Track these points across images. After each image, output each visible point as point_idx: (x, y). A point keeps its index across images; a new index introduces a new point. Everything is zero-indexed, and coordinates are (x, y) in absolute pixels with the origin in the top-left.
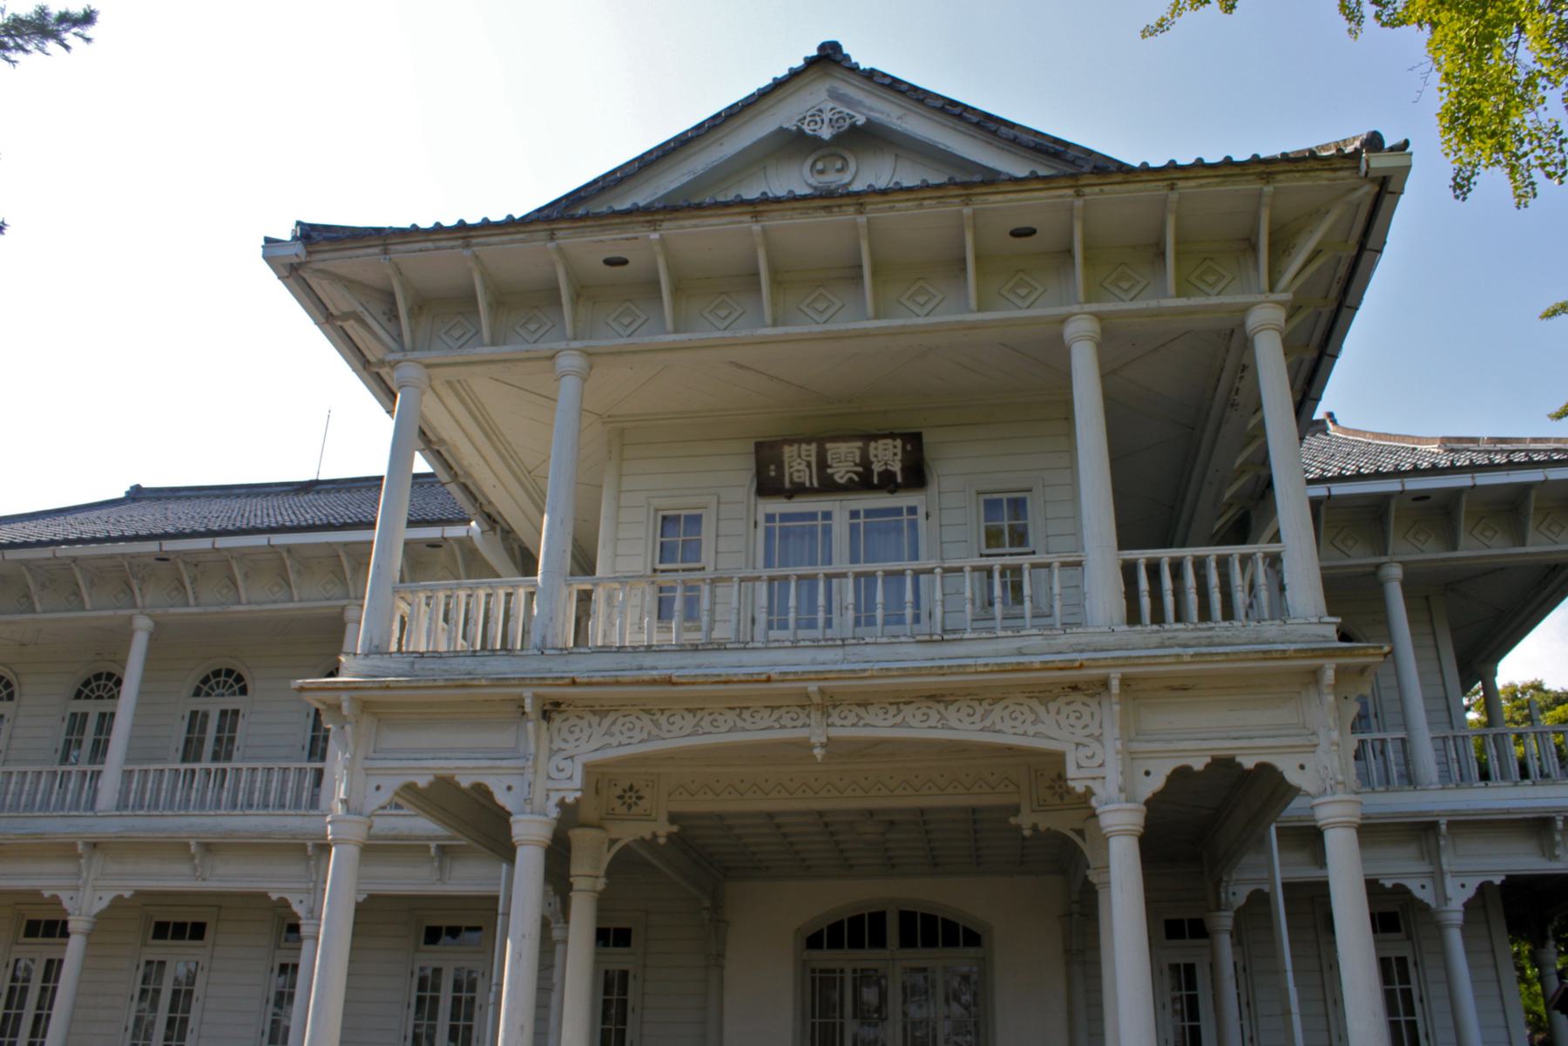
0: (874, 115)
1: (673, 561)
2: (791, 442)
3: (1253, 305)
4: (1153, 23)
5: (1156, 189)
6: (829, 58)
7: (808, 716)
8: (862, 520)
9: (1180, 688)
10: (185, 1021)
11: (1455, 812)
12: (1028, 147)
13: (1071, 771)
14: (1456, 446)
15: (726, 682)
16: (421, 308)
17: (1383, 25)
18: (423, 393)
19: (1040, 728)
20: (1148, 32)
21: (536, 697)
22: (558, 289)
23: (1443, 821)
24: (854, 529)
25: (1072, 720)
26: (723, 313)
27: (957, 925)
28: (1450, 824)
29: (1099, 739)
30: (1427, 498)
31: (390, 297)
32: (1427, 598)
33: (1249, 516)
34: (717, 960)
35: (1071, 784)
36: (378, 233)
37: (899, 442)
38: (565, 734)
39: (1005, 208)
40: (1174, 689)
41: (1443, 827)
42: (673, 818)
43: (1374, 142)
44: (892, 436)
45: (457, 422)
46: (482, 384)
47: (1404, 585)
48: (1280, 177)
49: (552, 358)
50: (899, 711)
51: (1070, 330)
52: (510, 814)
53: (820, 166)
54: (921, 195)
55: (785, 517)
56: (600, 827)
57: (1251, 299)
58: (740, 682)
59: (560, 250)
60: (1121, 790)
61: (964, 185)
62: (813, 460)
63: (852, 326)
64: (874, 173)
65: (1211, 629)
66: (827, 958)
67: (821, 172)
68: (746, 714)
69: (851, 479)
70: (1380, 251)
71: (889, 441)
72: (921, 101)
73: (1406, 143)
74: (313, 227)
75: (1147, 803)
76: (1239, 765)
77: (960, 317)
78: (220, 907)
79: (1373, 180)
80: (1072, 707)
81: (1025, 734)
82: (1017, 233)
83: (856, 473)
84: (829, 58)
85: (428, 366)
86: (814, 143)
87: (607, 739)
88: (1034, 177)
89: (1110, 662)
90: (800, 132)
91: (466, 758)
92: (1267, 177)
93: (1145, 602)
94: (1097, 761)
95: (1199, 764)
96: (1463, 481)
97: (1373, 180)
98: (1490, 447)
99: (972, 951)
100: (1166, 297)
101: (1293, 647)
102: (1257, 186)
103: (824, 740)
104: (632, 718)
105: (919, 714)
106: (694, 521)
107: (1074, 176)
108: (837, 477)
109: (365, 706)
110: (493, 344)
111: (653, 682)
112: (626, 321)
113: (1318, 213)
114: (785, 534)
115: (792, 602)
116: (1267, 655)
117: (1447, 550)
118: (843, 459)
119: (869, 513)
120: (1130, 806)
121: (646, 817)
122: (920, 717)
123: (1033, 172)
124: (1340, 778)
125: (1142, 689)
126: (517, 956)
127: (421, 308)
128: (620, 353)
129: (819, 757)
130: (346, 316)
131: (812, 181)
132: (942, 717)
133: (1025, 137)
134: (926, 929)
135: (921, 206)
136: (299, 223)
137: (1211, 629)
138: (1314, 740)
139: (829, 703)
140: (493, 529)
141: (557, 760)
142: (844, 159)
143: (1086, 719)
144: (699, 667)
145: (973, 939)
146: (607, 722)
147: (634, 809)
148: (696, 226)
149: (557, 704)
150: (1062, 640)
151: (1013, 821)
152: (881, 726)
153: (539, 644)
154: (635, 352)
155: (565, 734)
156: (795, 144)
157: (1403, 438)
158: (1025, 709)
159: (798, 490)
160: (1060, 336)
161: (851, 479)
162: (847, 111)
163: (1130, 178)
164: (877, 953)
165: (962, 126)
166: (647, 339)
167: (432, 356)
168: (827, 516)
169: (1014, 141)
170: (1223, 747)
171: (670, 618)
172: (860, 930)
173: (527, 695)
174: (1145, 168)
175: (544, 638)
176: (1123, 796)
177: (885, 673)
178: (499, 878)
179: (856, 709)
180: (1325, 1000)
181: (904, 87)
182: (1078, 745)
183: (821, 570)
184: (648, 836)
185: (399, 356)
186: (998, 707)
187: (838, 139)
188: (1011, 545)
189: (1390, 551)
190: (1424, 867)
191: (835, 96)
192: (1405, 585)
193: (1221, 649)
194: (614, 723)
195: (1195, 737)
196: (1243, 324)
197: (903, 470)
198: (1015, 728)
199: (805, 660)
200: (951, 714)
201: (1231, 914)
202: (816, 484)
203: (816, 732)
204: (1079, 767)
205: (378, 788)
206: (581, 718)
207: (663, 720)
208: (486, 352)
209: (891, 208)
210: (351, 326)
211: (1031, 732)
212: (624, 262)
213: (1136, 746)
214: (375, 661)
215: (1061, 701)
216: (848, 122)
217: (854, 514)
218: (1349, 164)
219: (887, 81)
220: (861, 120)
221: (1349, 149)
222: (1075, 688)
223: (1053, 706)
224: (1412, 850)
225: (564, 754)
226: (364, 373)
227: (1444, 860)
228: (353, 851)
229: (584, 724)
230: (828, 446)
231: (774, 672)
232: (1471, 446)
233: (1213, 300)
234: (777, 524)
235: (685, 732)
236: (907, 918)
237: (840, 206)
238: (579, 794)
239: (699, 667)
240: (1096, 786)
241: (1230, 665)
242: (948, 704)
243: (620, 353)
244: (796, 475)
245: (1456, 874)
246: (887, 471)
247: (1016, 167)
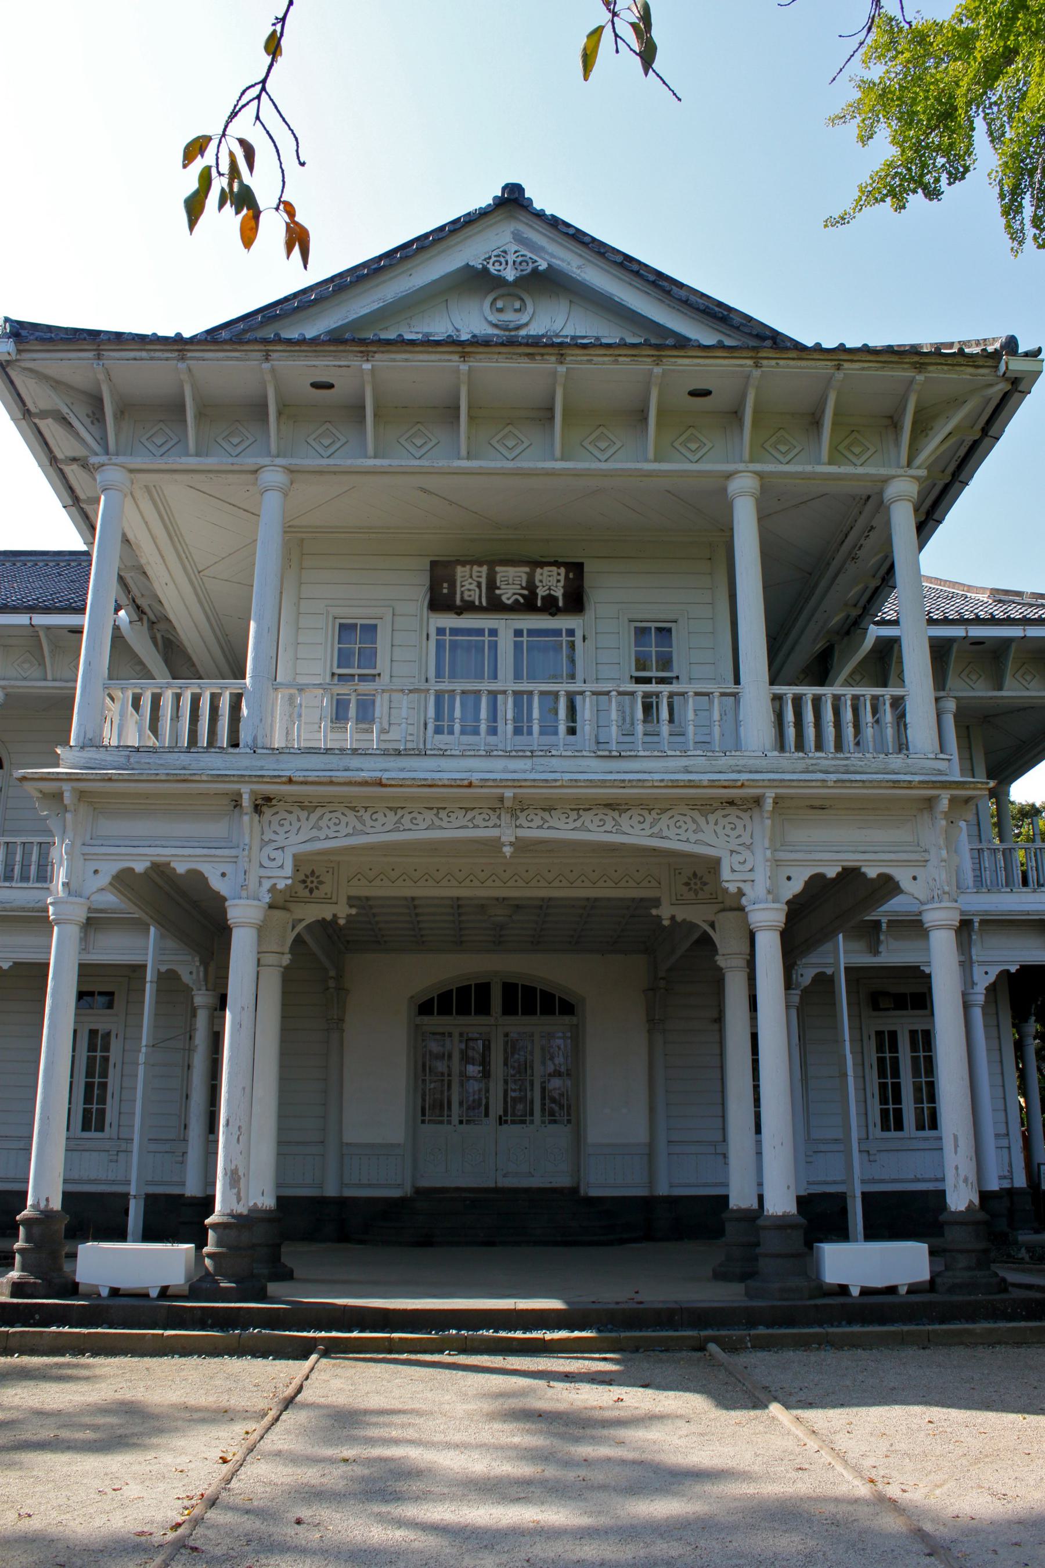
0: (556, 262)
1: (348, 666)
2: (464, 564)
3: (894, 477)
4: (836, 215)
5: (823, 367)
6: (513, 200)
7: (499, 817)
8: (525, 639)
9: (819, 807)
10: (104, 1086)
11: (987, 913)
12: (698, 309)
13: (726, 874)
14: (1003, 597)
15: (430, 786)
16: (122, 412)
17: (1039, 247)
18: (125, 496)
19: (700, 836)
20: (831, 223)
21: (253, 792)
22: (266, 406)
23: (976, 919)
24: (518, 646)
25: (728, 831)
26: (419, 442)
27: (554, 996)
29: (749, 847)
30: (983, 643)
31: (97, 402)
32: (968, 727)
33: (885, 661)
34: (336, 1024)
35: (726, 885)
36: (94, 335)
37: (562, 570)
38: (275, 826)
39: (691, 371)
40: (813, 807)
41: (976, 924)
42: (352, 901)
43: (1011, 345)
44: (556, 564)
45: (146, 523)
46: (177, 493)
47: (956, 716)
48: (931, 368)
49: (256, 471)
50: (580, 816)
51: (735, 486)
52: (225, 899)
53: (500, 304)
54: (617, 352)
55: (455, 632)
57: (892, 472)
58: (444, 786)
59: (273, 370)
60: (769, 892)
61: (658, 347)
62: (483, 581)
63: (541, 465)
64: (548, 319)
65: (847, 758)
66: (435, 1022)
67: (500, 310)
68: (443, 814)
69: (517, 600)
70: (998, 439)
71: (554, 568)
72: (602, 255)
73: (1039, 350)
74: (20, 323)
75: (788, 903)
76: (864, 875)
77: (639, 466)
79: (1007, 379)
80: (729, 819)
81: (687, 841)
82: (694, 394)
83: (520, 595)
84: (513, 200)
85: (131, 471)
86: (499, 282)
87: (314, 833)
88: (720, 346)
89: (766, 783)
90: (485, 270)
91: (184, 848)
92: (920, 367)
93: (791, 732)
94: (748, 866)
96: (1016, 632)
97: (1007, 379)
98: (1033, 601)
99: (567, 1019)
100: (819, 463)
101: (917, 778)
102: (910, 374)
103: (513, 839)
104: (338, 814)
105: (596, 819)
106: (371, 630)
107: (755, 349)
108: (504, 598)
109: (82, 795)
110: (198, 454)
111: (365, 783)
112: (326, 442)
113: (956, 402)
114: (454, 645)
115: (458, 713)
116: (896, 784)
117: (994, 690)
118: (511, 582)
119: (531, 633)
120: (776, 905)
121: (327, 900)
122: (597, 822)
123: (720, 341)
124: (947, 889)
125: (796, 807)
126: (237, 1026)
127: (122, 412)
128: (321, 473)
129: (508, 855)
130: (44, 414)
131: (492, 318)
132: (617, 823)
133: (693, 298)
134: (528, 1000)
135: (616, 362)
136: (7, 320)
137: (847, 758)
138: (927, 856)
139: (520, 807)
140: (141, 620)
141: (268, 850)
142: (522, 300)
143: (740, 830)
144: (402, 770)
145: (568, 1008)
146: (314, 817)
147: (316, 892)
148: (406, 360)
149: (268, 799)
150: (723, 762)
151: (654, 912)
152: (562, 829)
153: (250, 743)
154: (335, 473)
155: (275, 826)
156: (478, 281)
157: (954, 584)
158: (688, 819)
159: (469, 607)
160: (725, 490)
161: (517, 600)
162: (529, 255)
163: (804, 355)
164: (482, 1019)
165: (637, 282)
166: (349, 462)
167: (137, 462)
168: (493, 632)
169: (686, 302)
170: (851, 859)
171: (347, 719)
172: (463, 1000)
173: (245, 790)
174: (818, 348)
175: (255, 739)
176: (770, 897)
177: (574, 783)
178: (147, 949)
179: (541, 813)
180: (863, 1064)
181: (587, 239)
182: (732, 852)
183: (485, 686)
184: (329, 918)
185: (103, 459)
186: (665, 817)
187: (518, 281)
188: (657, 670)
189: (947, 688)
191: (518, 238)
192: (957, 717)
193: (858, 777)
194: (321, 818)
195: (829, 849)
196: (881, 493)
197: (564, 595)
198: (680, 836)
199: (498, 769)
200: (624, 820)
201: (798, 992)
202: (484, 603)
204: (733, 871)
205: (96, 872)
206: (291, 813)
207: (366, 817)
208: (192, 462)
209: (590, 361)
210: (48, 426)
211: (693, 839)
212: (331, 386)
213: (782, 855)
214: (90, 754)
215: (719, 813)
216: (531, 266)
217: (518, 633)
218: (990, 363)
219: (571, 231)
220: (543, 266)
221: (990, 349)
222: (731, 803)
223: (712, 818)
225: (274, 845)
226: (51, 470)
227: (974, 952)
228: (74, 932)
229: (293, 817)
230: (498, 569)
231: (475, 777)
232: (1017, 599)
233: (860, 470)
234: (448, 638)
235: (387, 828)
236: (509, 989)
237: (542, 355)
238: (289, 882)
239: (402, 770)
240: (746, 888)
241: (865, 791)
243: (321, 473)
244: (466, 593)
246: (550, 595)
247: (706, 336)
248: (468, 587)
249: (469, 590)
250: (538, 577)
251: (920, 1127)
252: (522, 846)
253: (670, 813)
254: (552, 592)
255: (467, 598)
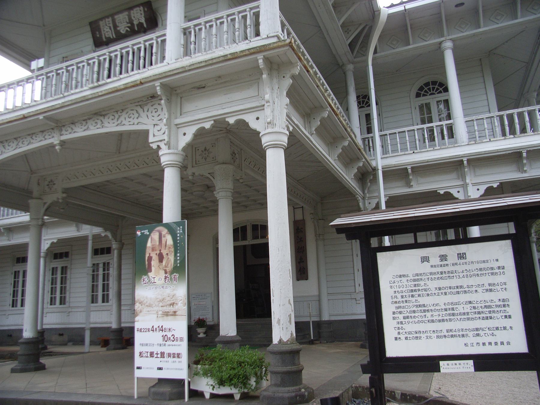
2: (101, 19)
13: (151, 139)
19: (140, 120)
23: (465, 159)
28: (468, 160)
37: (142, 8)
41: (465, 162)
44: (138, 6)
56: (40, 199)
62: (111, 25)
69: (127, 31)
71: (138, 8)
78: (72, 246)
80: (154, 107)
83: (128, 27)
95: (207, 125)
158: (135, 112)
184: (55, 199)
190: (460, 183)
197: (146, 21)
203: (55, 140)
212: (463, 4)
224: (454, 175)
230: (116, 17)
242: (104, 116)
244: (106, 34)
245: (474, 184)
248: (106, 30)
249: (107, 32)
250: (132, 15)
251: (103, 302)
252: (63, 143)
253: (125, 112)
254: (141, 21)
255: (107, 36)
